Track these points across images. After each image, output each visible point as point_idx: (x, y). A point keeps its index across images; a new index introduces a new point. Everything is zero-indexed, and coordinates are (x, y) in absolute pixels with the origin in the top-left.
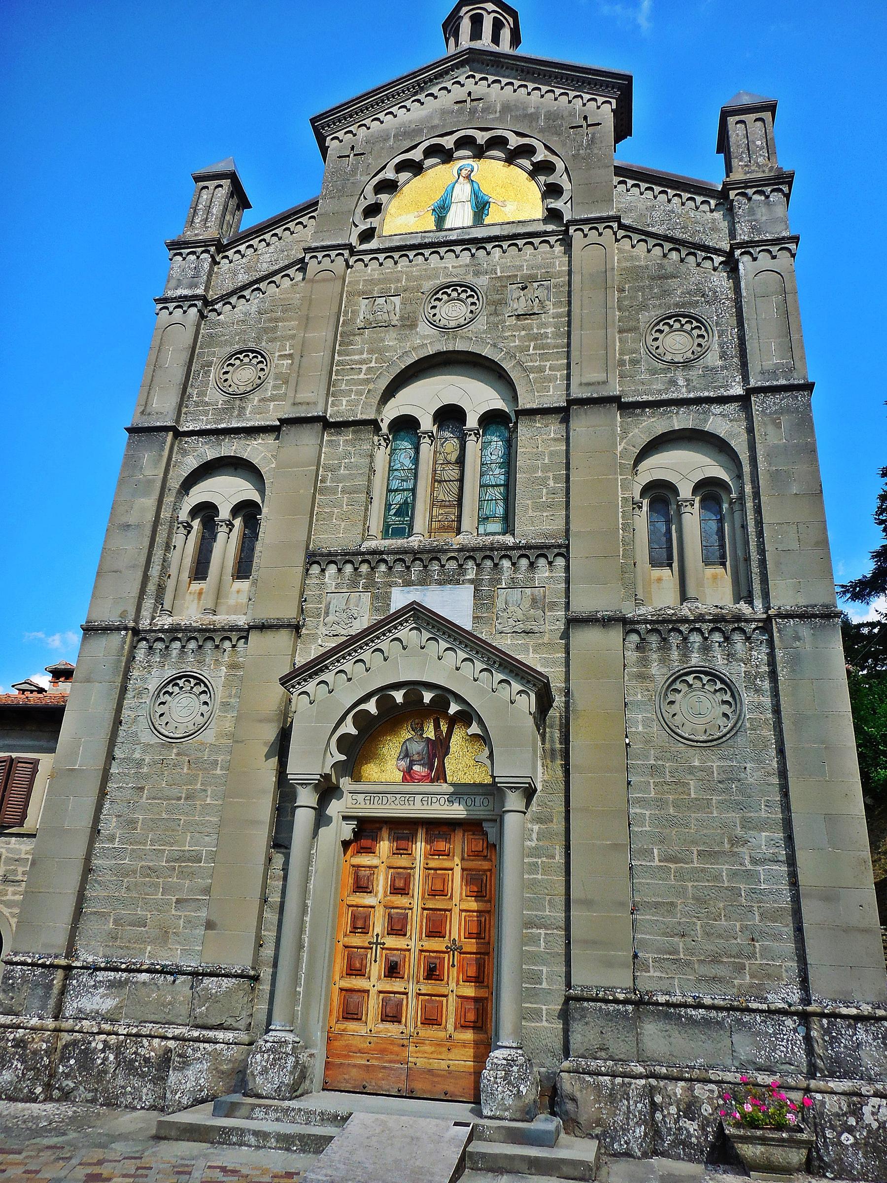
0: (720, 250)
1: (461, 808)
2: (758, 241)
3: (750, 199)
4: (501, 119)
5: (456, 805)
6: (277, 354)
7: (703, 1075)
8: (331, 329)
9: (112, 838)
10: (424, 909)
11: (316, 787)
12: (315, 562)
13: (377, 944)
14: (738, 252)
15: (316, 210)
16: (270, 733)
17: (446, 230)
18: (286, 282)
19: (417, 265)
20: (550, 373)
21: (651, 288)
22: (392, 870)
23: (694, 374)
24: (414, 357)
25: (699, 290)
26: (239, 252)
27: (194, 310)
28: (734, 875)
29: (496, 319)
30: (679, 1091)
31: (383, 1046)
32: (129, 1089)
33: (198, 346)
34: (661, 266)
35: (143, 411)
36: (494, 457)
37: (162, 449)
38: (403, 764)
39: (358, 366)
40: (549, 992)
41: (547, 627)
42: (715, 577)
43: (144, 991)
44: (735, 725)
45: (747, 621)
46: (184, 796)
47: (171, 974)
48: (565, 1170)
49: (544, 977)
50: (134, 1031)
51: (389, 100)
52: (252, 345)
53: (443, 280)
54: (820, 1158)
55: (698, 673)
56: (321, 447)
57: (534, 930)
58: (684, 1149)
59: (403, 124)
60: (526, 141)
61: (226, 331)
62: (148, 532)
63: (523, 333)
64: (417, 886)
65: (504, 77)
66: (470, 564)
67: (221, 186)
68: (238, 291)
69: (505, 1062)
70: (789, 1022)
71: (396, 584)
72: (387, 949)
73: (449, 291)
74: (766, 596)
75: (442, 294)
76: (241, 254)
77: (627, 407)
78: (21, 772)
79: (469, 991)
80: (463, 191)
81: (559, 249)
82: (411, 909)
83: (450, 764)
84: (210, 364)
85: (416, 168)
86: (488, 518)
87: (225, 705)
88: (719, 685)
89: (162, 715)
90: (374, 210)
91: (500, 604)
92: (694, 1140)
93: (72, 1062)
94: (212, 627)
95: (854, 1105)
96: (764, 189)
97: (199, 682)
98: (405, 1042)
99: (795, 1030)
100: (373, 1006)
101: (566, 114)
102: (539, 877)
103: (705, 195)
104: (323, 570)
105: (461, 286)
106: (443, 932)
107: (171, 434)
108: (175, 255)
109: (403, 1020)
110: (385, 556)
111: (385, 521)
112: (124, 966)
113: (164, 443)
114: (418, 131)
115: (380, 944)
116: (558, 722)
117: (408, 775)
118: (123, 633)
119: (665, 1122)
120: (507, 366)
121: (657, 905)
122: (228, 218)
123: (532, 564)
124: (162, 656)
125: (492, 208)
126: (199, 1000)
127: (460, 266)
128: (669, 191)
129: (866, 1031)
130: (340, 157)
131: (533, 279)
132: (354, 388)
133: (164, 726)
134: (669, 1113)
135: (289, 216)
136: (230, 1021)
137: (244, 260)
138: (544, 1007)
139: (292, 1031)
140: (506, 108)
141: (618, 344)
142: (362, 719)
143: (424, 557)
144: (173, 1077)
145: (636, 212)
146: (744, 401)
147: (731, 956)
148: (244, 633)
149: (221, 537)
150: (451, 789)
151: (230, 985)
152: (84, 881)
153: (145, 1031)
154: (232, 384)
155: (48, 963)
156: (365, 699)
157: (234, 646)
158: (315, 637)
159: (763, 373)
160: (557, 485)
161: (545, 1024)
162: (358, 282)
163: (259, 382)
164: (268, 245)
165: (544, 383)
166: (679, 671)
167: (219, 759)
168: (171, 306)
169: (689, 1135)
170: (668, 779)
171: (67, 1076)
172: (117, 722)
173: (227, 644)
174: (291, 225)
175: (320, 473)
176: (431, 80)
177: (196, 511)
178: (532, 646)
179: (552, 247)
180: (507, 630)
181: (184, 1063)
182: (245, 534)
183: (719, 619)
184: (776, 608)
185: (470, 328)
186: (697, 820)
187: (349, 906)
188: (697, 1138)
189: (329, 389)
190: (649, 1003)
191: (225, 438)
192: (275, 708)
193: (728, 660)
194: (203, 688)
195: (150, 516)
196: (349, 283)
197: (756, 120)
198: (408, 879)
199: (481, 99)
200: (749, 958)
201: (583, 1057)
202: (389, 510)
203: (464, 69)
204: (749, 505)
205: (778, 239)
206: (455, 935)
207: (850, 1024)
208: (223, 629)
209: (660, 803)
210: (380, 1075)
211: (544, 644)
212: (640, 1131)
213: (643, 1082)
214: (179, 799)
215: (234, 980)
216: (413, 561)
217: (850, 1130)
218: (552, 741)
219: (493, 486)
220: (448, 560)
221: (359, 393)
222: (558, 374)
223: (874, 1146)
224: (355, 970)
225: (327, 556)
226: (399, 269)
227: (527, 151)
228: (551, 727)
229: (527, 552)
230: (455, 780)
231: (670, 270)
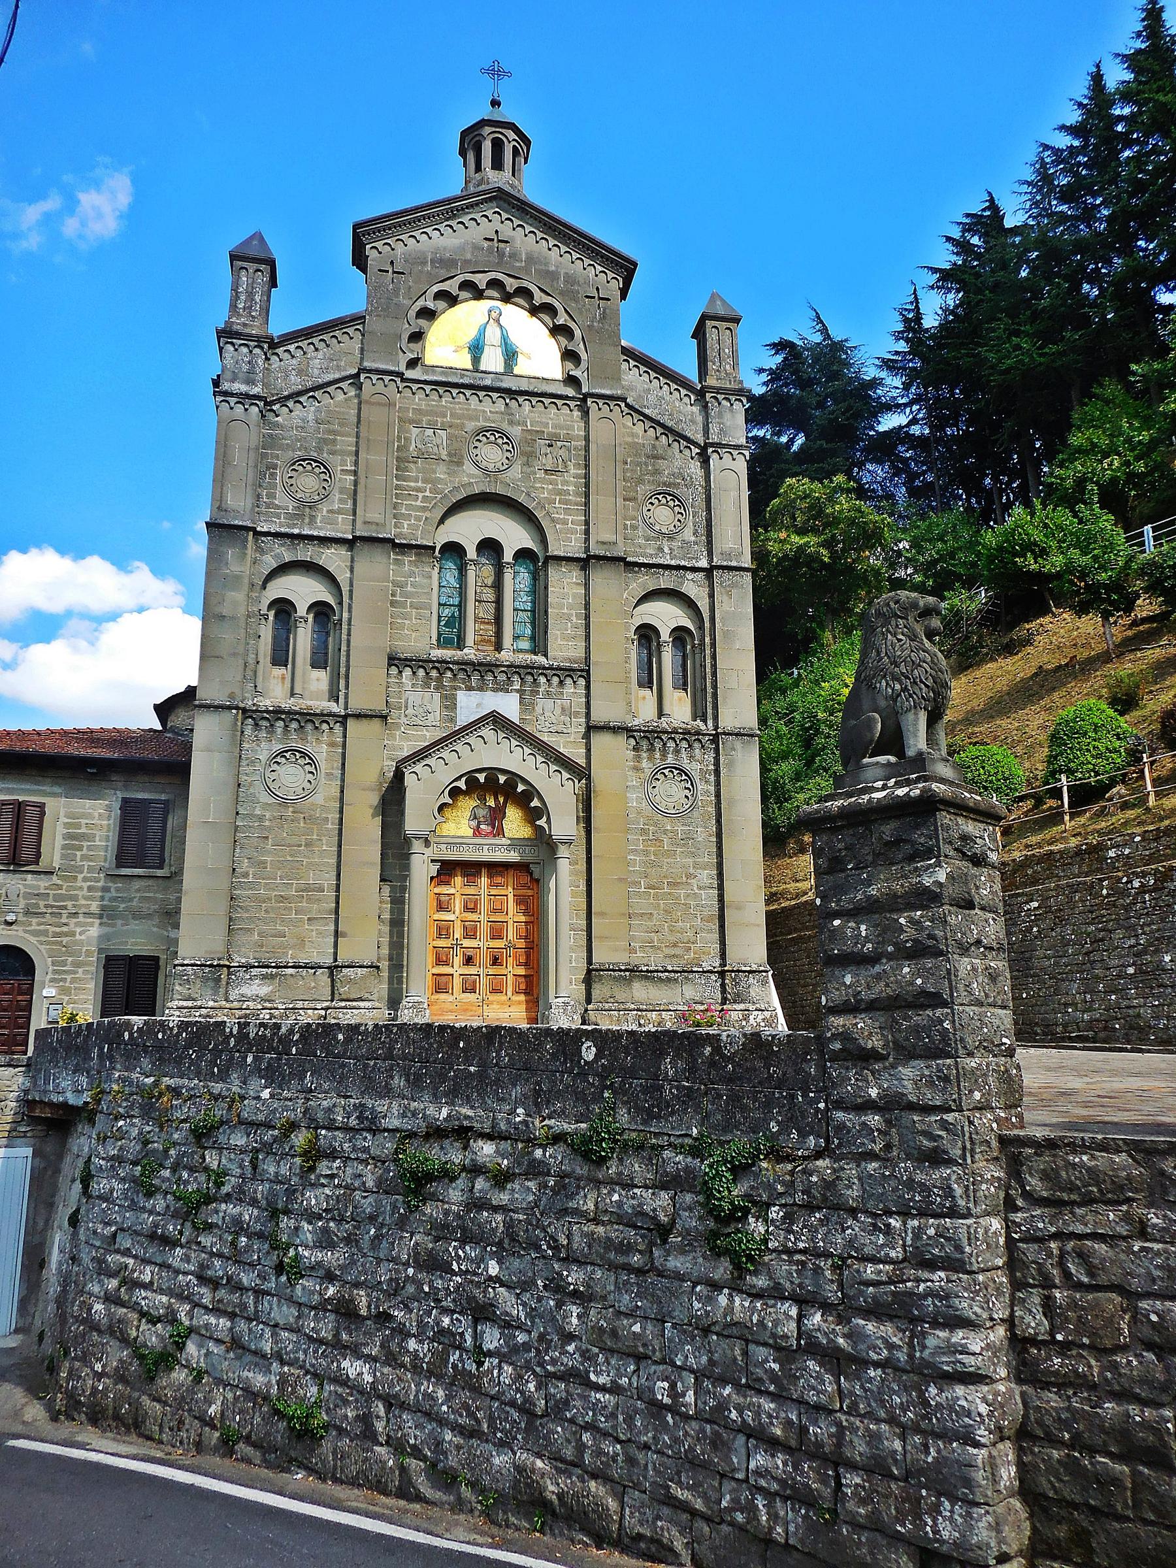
3: (720, 404)
9: (246, 875)
14: (710, 450)
17: (483, 372)
18: (340, 397)
23: (676, 544)
24: (462, 494)
29: (529, 470)
37: (245, 547)
38: (474, 823)
41: (573, 730)
43: (291, 981)
47: (312, 968)
59: (437, 250)
60: (548, 300)
61: (287, 434)
66: (516, 678)
70: (713, 977)
73: (488, 434)
74: (716, 718)
77: (631, 566)
78: (31, 814)
79: (521, 971)
84: (275, 467)
91: (538, 709)
101: (582, 281)
104: (400, 672)
117: (477, 832)
120: (539, 514)
123: (561, 682)
125: (520, 359)
132: (413, 514)
135: (337, 325)
136: (366, 995)
137: (294, 361)
146: (709, 572)
168: (233, 400)
176: (463, 209)
180: (545, 730)
183: (686, 732)
194: (308, 761)
204: (708, 652)
206: (510, 937)
208: (322, 715)
209: (646, 853)
214: (300, 846)
221: (418, 519)
230: (511, 836)
231: (660, 452)
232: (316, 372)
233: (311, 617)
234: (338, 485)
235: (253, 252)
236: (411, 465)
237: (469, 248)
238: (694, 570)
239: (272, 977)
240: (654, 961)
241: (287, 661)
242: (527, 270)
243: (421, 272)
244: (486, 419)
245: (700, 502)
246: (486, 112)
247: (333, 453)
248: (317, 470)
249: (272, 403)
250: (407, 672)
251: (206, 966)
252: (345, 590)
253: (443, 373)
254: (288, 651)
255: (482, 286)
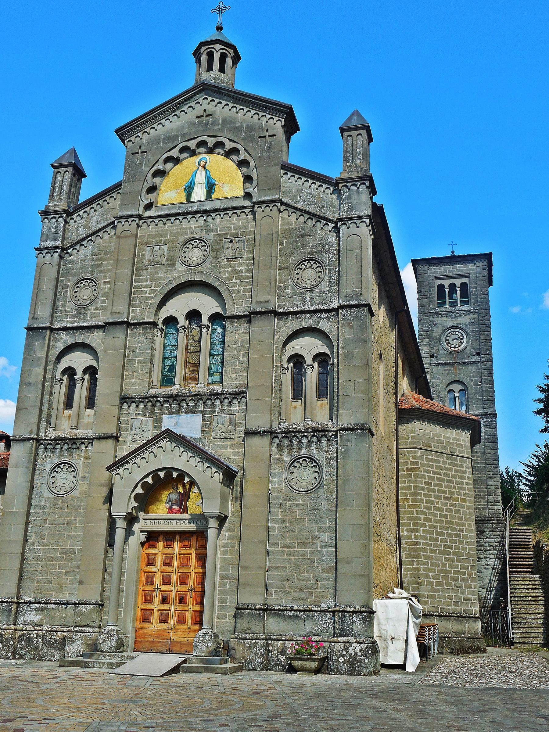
0: (332, 220)
1: (194, 525)
2: (350, 218)
3: (349, 189)
4: (222, 130)
5: (192, 524)
6: (102, 281)
7: (291, 638)
8: (130, 267)
10: (179, 573)
11: (125, 519)
12: (125, 402)
13: (157, 589)
14: (340, 223)
15: (121, 188)
16: (105, 492)
18: (106, 236)
19: (176, 226)
20: (243, 294)
21: (297, 242)
22: (164, 555)
25: (321, 244)
26: (79, 215)
27: (56, 255)
28: (312, 553)
29: (216, 261)
30: (279, 645)
31: (160, 633)
32: (49, 653)
33: (60, 276)
34: (303, 229)
35: (33, 317)
36: (218, 338)
38: (168, 505)
39: (145, 289)
40: (230, 607)
41: (236, 435)
42: (322, 405)
43: (53, 612)
44: (319, 483)
45: (328, 431)
46: (66, 523)
47: (64, 604)
48: (218, 671)
49: (228, 600)
50: (50, 629)
51: (159, 116)
52: (89, 275)
53: (189, 236)
54: (331, 668)
55: (305, 458)
56: (126, 338)
57: (225, 581)
58: (278, 667)
59: (167, 132)
61: (75, 266)
62: (40, 387)
63: (230, 269)
64: (176, 562)
65: (224, 100)
67: (67, 171)
68: (80, 242)
69: (203, 634)
70: (329, 615)
71: (165, 413)
72: (162, 591)
75: (189, 244)
76: (80, 217)
80: (201, 176)
81: (250, 217)
82: (173, 573)
83: (190, 505)
85: (176, 161)
86: (214, 373)
87: (83, 477)
88: (314, 464)
89: (53, 483)
90: (152, 189)
91: (214, 423)
92: (283, 663)
93: (23, 643)
94: (75, 437)
95: (347, 646)
96: (357, 183)
97: (71, 466)
98: (170, 631)
99: (331, 619)
100: (156, 616)
101: (257, 127)
102: (228, 556)
103: (328, 184)
104: (129, 407)
105: (199, 240)
106: (187, 582)
107: (48, 331)
108: (45, 218)
109: (169, 622)
110: (159, 399)
111: (162, 375)
112: (43, 602)
113: (46, 336)
114: (176, 137)
115: (159, 589)
116: (239, 484)
118: (32, 441)
119: (272, 657)
120: (221, 289)
121: (278, 568)
122: (72, 190)
123: (230, 403)
124: (52, 453)
125: (216, 189)
126: (77, 615)
127: (199, 227)
128: (310, 180)
129: (357, 617)
130: (133, 154)
131: (236, 235)
133: (54, 488)
134: (274, 654)
135: (106, 193)
136: (91, 624)
137: (83, 221)
138: (227, 613)
139: (117, 626)
140: (225, 122)
141: (278, 276)
142: (145, 486)
143: (178, 399)
144: (67, 647)
145: (292, 193)
147: (308, 589)
148: (91, 440)
149: (78, 386)
150: (190, 517)
151: (90, 608)
152: (22, 564)
153: (54, 629)
154: (80, 299)
155: (9, 601)
156: (147, 476)
157: (86, 447)
158: (125, 442)
159: (346, 297)
160: (244, 359)
161: (227, 620)
162: (144, 236)
163: (94, 298)
164: (95, 211)
165: (240, 299)
166: (296, 457)
167: (82, 504)
169: (281, 662)
170: (287, 510)
171: (21, 649)
172: (32, 487)
173: (83, 446)
174: (107, 198)
175: (127, 352)
176: (183, 103)
177: (64, 372)
178: (229, 445)
179: (247, 215)
181: (72, 641)
182: (91, 383)
184: (341, 425)
185: (203, 266)
186: (299, 528)
187: (145, 572)
188: (284, 662)
189: (130, 303)
190: (271, 610)
191: (77, 332)
192: (107, 479)
193: (319, 451)
194: (314, 464)
195: (41, 378)
196: (140, 237)
197: (358, 135)
198: (171, 559)
199: (211, 115)
200: (315, 589)
201: (240, 632)
202: (165, 369)
203: (202, 94)
205: (359, 217)
207: (350, 615)
208: (81, 439)
210: (158, 645)
211: (234, 444)
212: (260, 660)
213: (264, 641)
214: (64, 524)
215: (92, 606)
216: (173, 401)
217: (343, 656)
218: (236, 493)
219: (217, 355)
220: (190, 401)
222: (247, 294)
223: (351, 662)
224: (148, 600)
225: (131, 399)
226: (166, 228)
227: (235, 151)
228: (236, 486)
229: (228, 396)
232: (94, 224)
233: (316, 364)
234: (101, 292)
235: (354, 123)
236: (144, 272)
237: (186, 126)
238: (327, 311)
239: (42, 610)
240: (285, 602)
241: (302, 396)
242: (222, 130)
243: (156, 149)
244: (192, 233)
245: (334, 262)
246: (213, 35)
247: (99, 272)
248: (314, 266)
249: (68, 248)
250: (133, 406)
251: (5, 602)
252: (335, 343)
253: (169, 209)
254: (302, 389)
255: (210, 145)
